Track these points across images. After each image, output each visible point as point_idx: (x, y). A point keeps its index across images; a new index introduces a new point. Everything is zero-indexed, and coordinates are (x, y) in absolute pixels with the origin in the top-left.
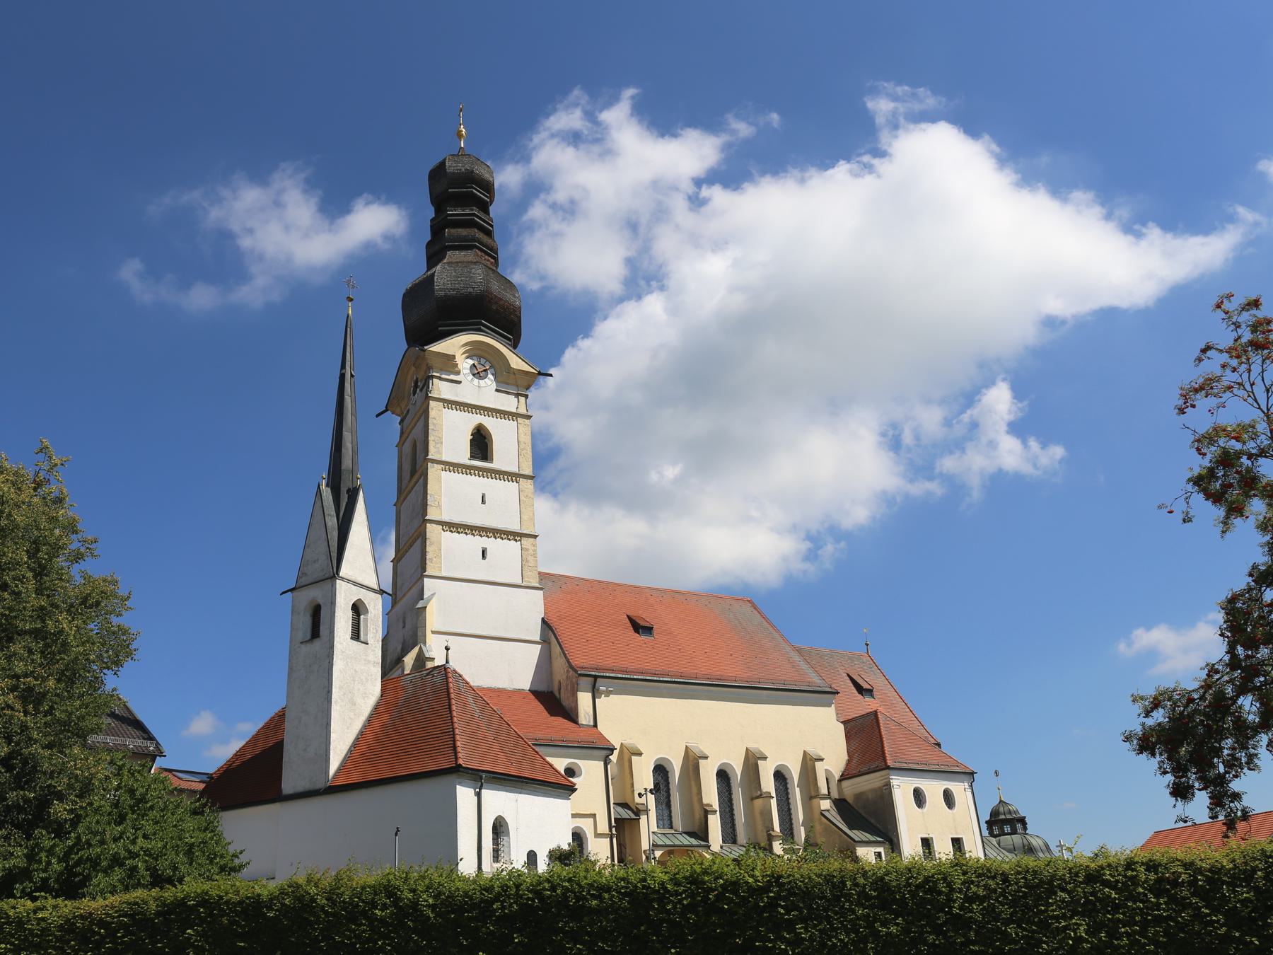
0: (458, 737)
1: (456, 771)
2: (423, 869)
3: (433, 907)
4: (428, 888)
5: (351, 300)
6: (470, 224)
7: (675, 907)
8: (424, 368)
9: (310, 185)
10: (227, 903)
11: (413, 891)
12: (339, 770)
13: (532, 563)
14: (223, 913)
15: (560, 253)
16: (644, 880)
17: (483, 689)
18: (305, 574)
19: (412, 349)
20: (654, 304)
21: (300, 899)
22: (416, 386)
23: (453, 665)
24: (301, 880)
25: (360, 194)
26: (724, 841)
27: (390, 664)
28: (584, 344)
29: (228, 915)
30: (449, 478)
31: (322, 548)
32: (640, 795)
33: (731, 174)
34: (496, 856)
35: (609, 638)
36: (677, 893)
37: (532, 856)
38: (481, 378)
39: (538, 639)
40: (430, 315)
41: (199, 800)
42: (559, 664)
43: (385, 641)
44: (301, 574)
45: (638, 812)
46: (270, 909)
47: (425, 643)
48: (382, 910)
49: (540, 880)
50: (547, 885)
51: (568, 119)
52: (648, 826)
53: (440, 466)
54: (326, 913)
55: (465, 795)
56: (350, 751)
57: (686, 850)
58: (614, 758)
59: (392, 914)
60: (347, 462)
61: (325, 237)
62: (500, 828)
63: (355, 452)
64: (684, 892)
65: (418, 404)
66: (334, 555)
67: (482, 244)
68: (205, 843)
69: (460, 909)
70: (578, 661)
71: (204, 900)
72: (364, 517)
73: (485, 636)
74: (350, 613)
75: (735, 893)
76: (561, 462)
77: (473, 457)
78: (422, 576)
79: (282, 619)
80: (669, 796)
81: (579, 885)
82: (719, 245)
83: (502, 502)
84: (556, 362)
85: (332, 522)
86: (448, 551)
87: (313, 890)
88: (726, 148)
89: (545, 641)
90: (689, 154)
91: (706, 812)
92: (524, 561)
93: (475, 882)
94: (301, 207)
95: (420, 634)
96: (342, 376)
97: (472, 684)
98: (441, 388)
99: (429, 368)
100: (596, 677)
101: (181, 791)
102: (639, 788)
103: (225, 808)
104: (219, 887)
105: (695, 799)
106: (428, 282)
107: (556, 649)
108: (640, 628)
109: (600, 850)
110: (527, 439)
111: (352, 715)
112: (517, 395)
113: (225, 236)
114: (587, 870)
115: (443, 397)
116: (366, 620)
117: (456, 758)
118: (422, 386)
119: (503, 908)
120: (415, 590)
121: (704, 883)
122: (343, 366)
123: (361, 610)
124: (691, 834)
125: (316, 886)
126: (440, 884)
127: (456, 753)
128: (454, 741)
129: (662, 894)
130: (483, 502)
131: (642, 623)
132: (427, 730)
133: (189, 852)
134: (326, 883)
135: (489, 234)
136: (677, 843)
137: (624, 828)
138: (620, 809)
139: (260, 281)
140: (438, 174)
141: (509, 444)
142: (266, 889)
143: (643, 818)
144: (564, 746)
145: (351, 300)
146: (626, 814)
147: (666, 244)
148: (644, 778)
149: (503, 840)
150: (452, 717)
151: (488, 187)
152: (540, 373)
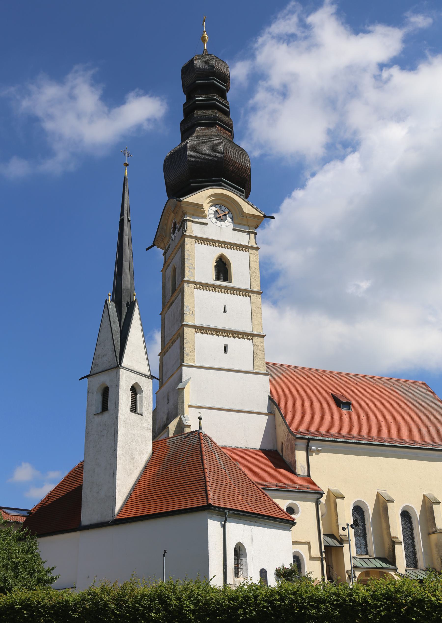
0: (208, 484)
1: (207, 508)
2: (186, 582)
3: (193, 612)
4: (190, 597)
5: (127, 165)
6: (212, 107)
7: (375, 617)
8: (180, 214)
9: (95, 81)
10: (43, 607)
11: (179, 599)
12: (122, 508)
13: (261, 356)
14: (40, 615)
15: (278, 126)
16: (351, 595)
17: (226, 448)
18: (96, 365)
19: (171, 200)
20: (353, 161)
21: (96, 604)
22: (175, 227)
23: (204, 430)
24: (97, 590)
25: (133, 89)
26: (408, 566)
27: (159, 430)
28: (298, 194)
29: (44, 616)
30: (200, 294)
31: (109, 345)
32: (343, 529)
33: (408, 59)
34: (237, 573)
35: (318, 411)
36: (376, 607)
37: (263, 573)
38: (222, 220)
39: (265, 411)
40: (186, 174)
41: (22, 530)
42: (282, 430)
43: (155, 412)
44: (94, 365)
45: (341, 541)
46: (75, 611)
47: (183, 414)
48: (157, 614)
49: (272, 593)
50: (277, 597)
51: (285, 25)
52: (350, 552)
53: (193, 286)
54: (115, 614)
55: (214, 526)
56: (130, 493)
57: (381, 573)
58: (323, 500)
59: (164, 616)
60: (126, 284)
61: (106, 121)
62: (239, 551)
63: (132, 276)
64: (382, 605)
65: (177, 240)
66: (118, 351)
67: (221, 121)
68: (27, 562)
69: (214, 614)
70: (296, 427)
71: (27, 605)
72: (139, 323)
73: (228, 410)
74: (130, 393)
75: (422, 608)
76: (280, 282)
77: (217, 278)
78: (181, 366)
79: (81, 397)
80: (365, 530)
81: (301, 597)
82: (400, 116)
83: (239, 312)
84: (277, 211)
85: (116, 327)
86: (200, 348)
87: (106, 598)
88: (406, 40)
89: (271, 413)
90: (379, 44)
91: (394, 543)
92: (254, 354)
93: (224, 593)
94: (88, 98)
95: (180, 407)
96: (122, 221)
97: (218, 444)
98: (193, 229)
99: (184, 214)
100: (309, 440)
101: (9, 523)
102: (342, 523)
103: (42, 535)
104: (38, 595)
105: (385, 532)
106: (182, 150)
107: (279, 419)
108: (340, 403)
109: (314, 570)
110: (256, 265)
111: (131, 467)
112: (249, 233)
113: (33, 120)
114: (308, 587)
115: (194, 235)
116: (141, 398)
117: (207, 499)
118: (179, 227)
119: (245, 613)
120: (176, 376)
121: (397, 599)
122: (122, 214)
123: (138, 390)
124: (383, 559)
125: (108, 595)
126: (198, 594)
127: (207, 495)
128: (206, 486)
129: (365, 606)
130: (225, 311)
131: (343, 400)
132: (185, 478)
133: (16, 568)
134: (115, 593)
135: (226, 113)
136: (372, 566)
137: (331, 553)
138: (328, 539)
139: (62, 156)
140: (188, 69)
141: (243, 268)
142: (73, 596)
143: (346, 546)
144: (286, 491)
145: (127, 165)
146: (333, 543)
147: (358, 116)
148: (346, 517)
149: (242, 561)
150: (204, 469)
151: (225, 79)
152: (265, 216)
